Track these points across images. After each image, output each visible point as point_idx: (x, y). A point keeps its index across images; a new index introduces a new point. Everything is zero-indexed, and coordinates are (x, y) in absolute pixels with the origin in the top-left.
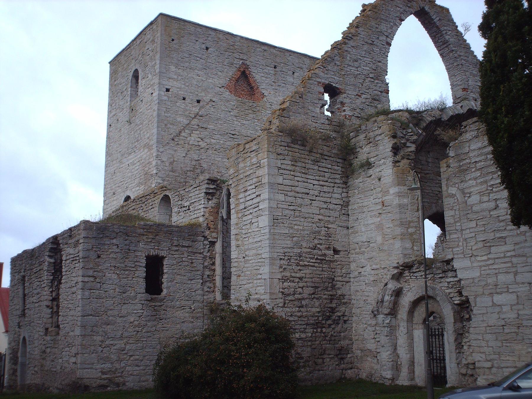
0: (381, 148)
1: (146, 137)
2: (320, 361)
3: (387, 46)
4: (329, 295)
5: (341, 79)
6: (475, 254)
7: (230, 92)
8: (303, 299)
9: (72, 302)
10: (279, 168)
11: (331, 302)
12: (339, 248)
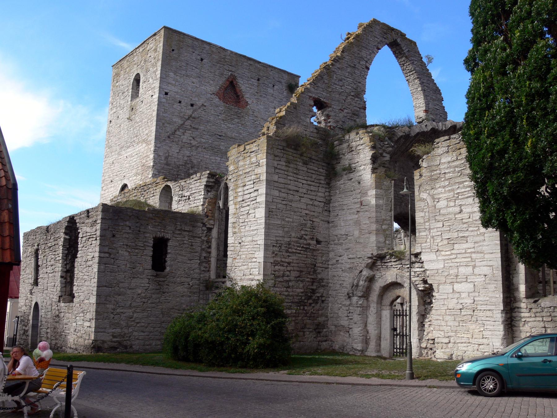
2: (301, 333)
3: (366, 70)
4: (311, 278)
5: (328, 95)
7: (220, 98)
8: (290, 281)
10: (276, 168)
11: (312, 285)
12: (321, 239)
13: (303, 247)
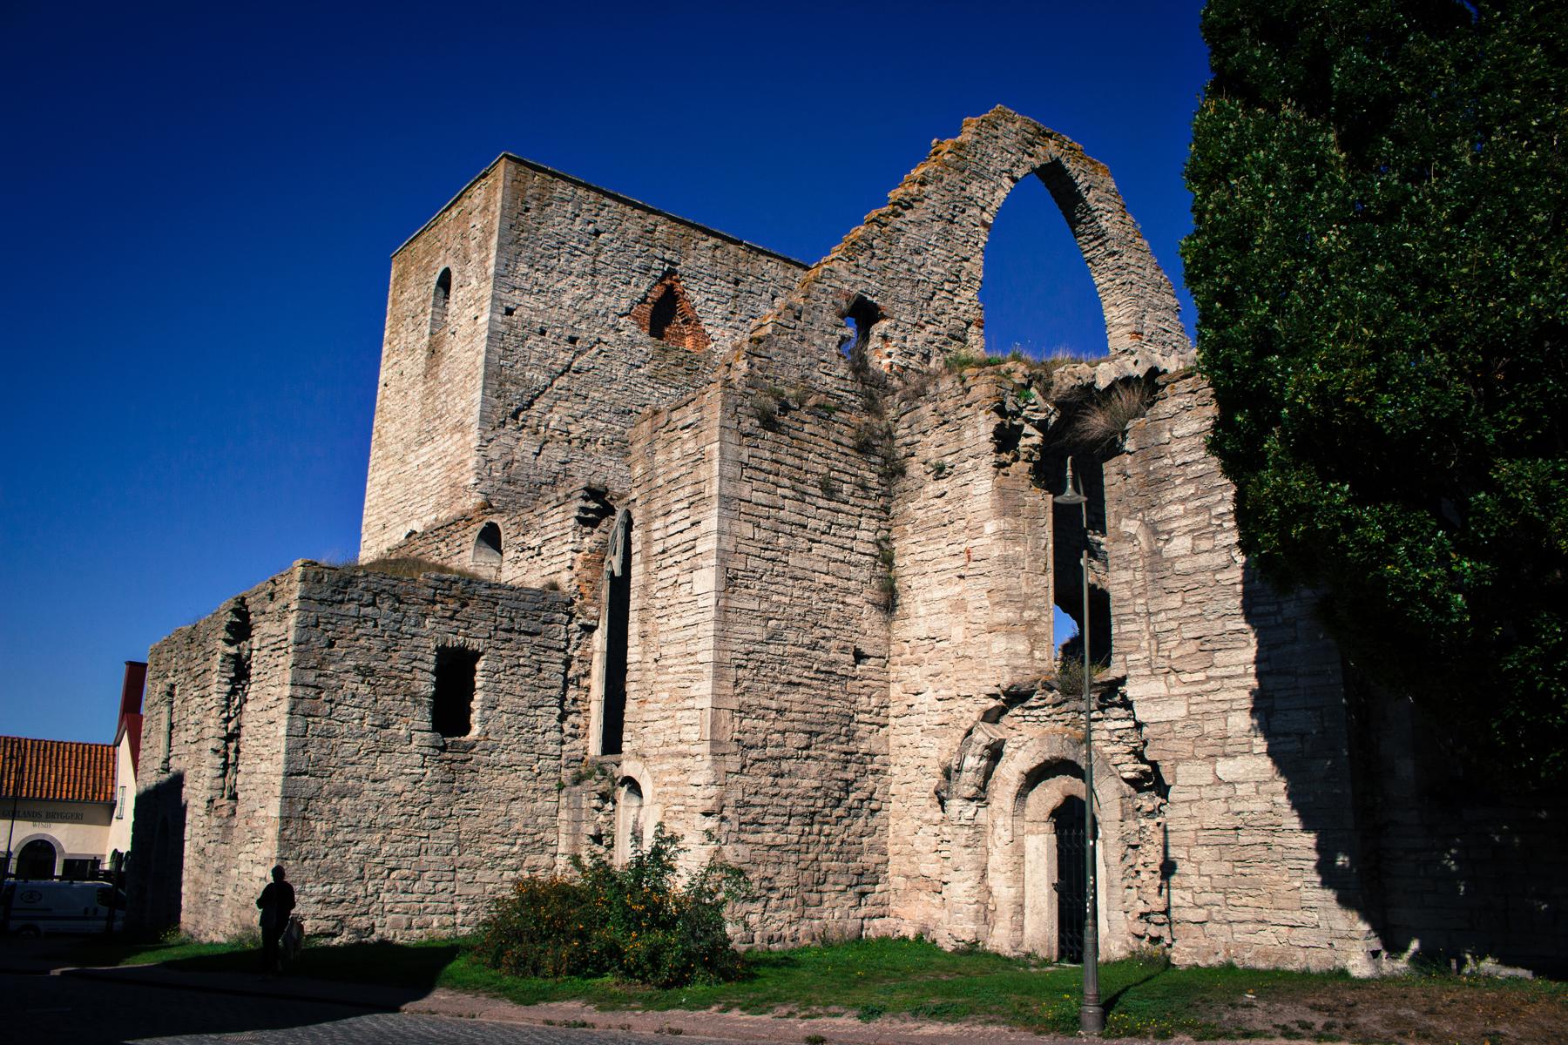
0: (968, 434)
1: (458, 408)
2: (815, 896)
6: (1177, 667)
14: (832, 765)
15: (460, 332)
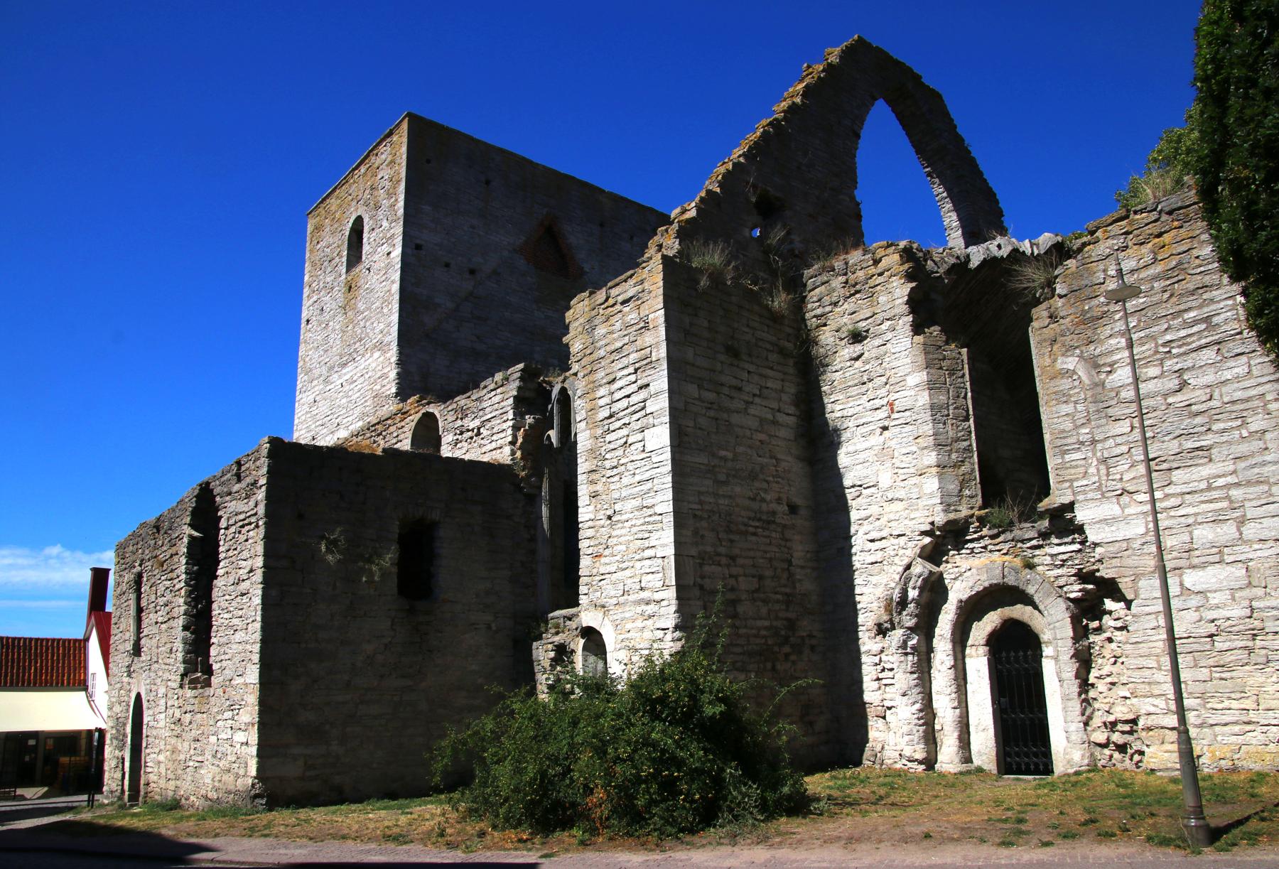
0: (882, 299)
1: (377, 331)
6: (1131, 489)
9: (240, 613)
13: (760, 520)
14: (777, 607)
15: (376, 266)
